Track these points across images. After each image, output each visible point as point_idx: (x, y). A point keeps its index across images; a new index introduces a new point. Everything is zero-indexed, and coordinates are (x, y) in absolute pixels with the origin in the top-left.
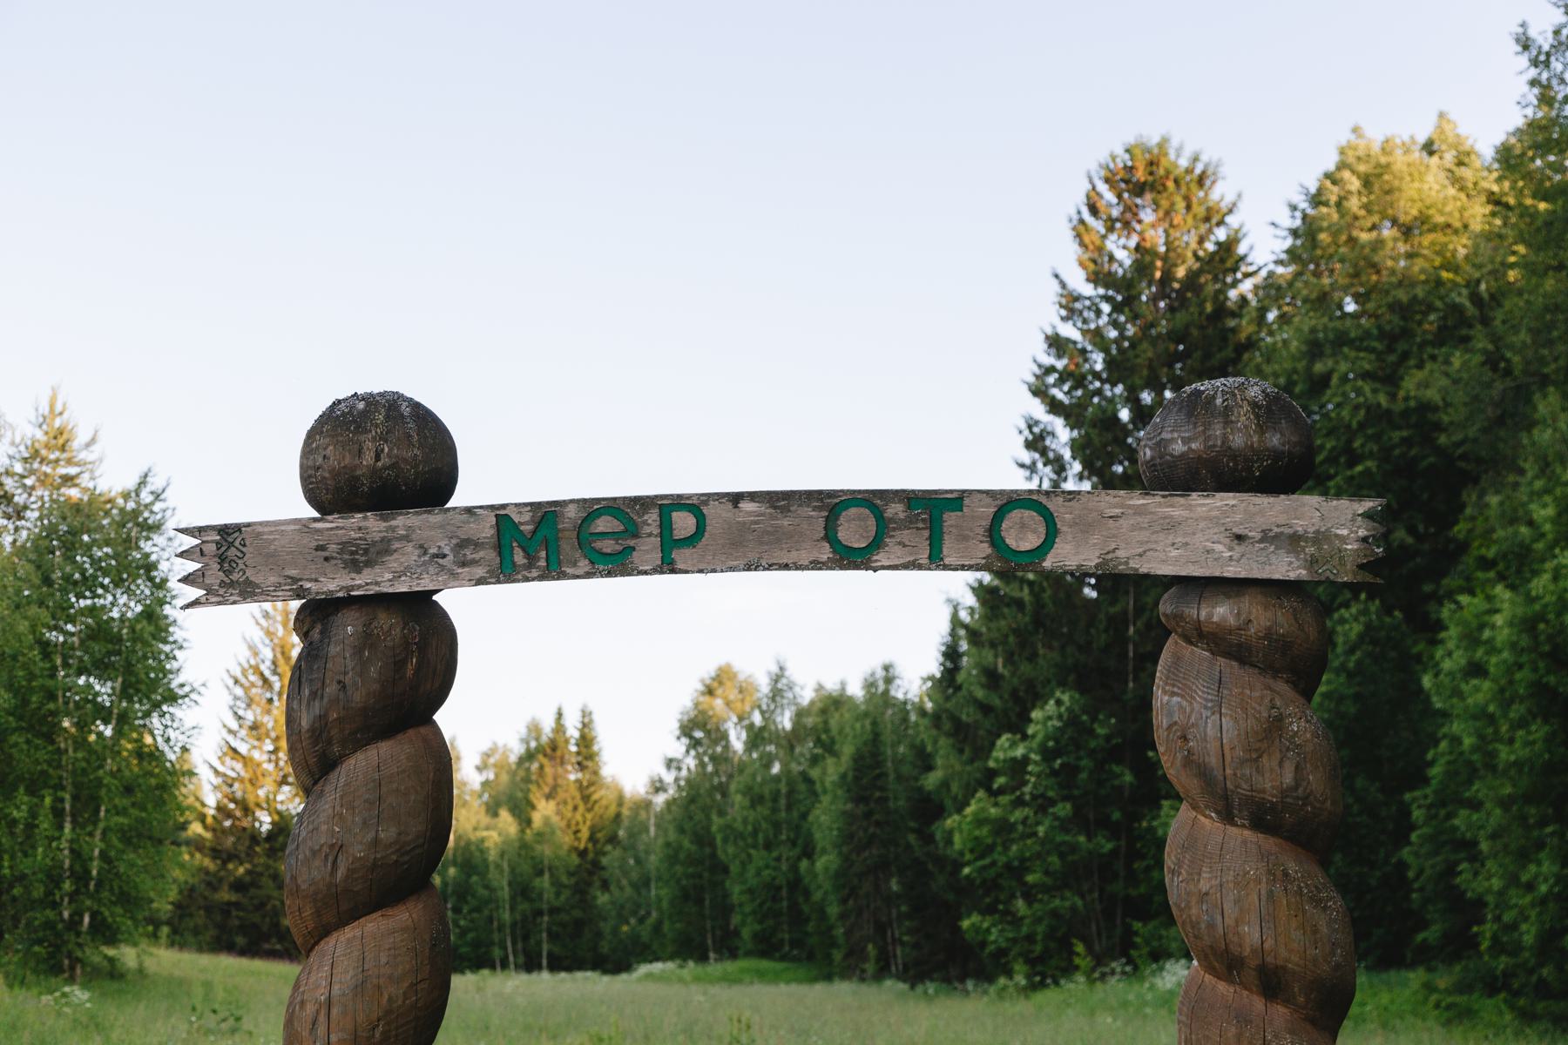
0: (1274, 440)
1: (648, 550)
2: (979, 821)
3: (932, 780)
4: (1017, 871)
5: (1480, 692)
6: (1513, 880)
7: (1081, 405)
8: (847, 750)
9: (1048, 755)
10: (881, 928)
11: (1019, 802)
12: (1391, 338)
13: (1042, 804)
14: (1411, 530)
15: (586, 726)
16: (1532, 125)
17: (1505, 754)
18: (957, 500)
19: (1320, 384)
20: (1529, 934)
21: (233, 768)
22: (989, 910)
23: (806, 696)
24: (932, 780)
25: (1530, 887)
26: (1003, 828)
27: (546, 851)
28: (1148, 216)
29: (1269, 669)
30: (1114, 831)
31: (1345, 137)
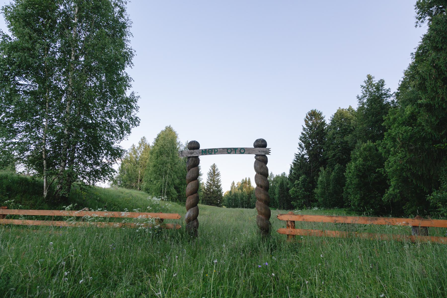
0: (263, 144)
1: (213, 152)
2: (293, 191)
3: (288, 186)
4: (298, 196)
5: (350, 175)
6: (354, 197)
7: (305, 141)
8: (279, 183)
9: (302, 183)
10: (284, 204)
11: (298, 188)
12: (343, 133)
13: (301, 188)
14: (346, 156)
15: (249, 179)
16: (360, 107)
17: (353, 182)
18: (237, 148)
19: (334, 138)
20: (356, 204)
21: (208, 184)
22: (294, 201)
23: (275, 176)
24: (288, 186)
25: (357, 198)
26: (296, 191)
27: (244, 194)
28: (313, 119)
29: (262, 162)
30: (309, 192)
31: (338, 109)
